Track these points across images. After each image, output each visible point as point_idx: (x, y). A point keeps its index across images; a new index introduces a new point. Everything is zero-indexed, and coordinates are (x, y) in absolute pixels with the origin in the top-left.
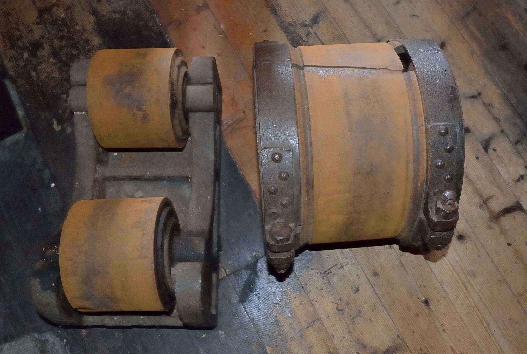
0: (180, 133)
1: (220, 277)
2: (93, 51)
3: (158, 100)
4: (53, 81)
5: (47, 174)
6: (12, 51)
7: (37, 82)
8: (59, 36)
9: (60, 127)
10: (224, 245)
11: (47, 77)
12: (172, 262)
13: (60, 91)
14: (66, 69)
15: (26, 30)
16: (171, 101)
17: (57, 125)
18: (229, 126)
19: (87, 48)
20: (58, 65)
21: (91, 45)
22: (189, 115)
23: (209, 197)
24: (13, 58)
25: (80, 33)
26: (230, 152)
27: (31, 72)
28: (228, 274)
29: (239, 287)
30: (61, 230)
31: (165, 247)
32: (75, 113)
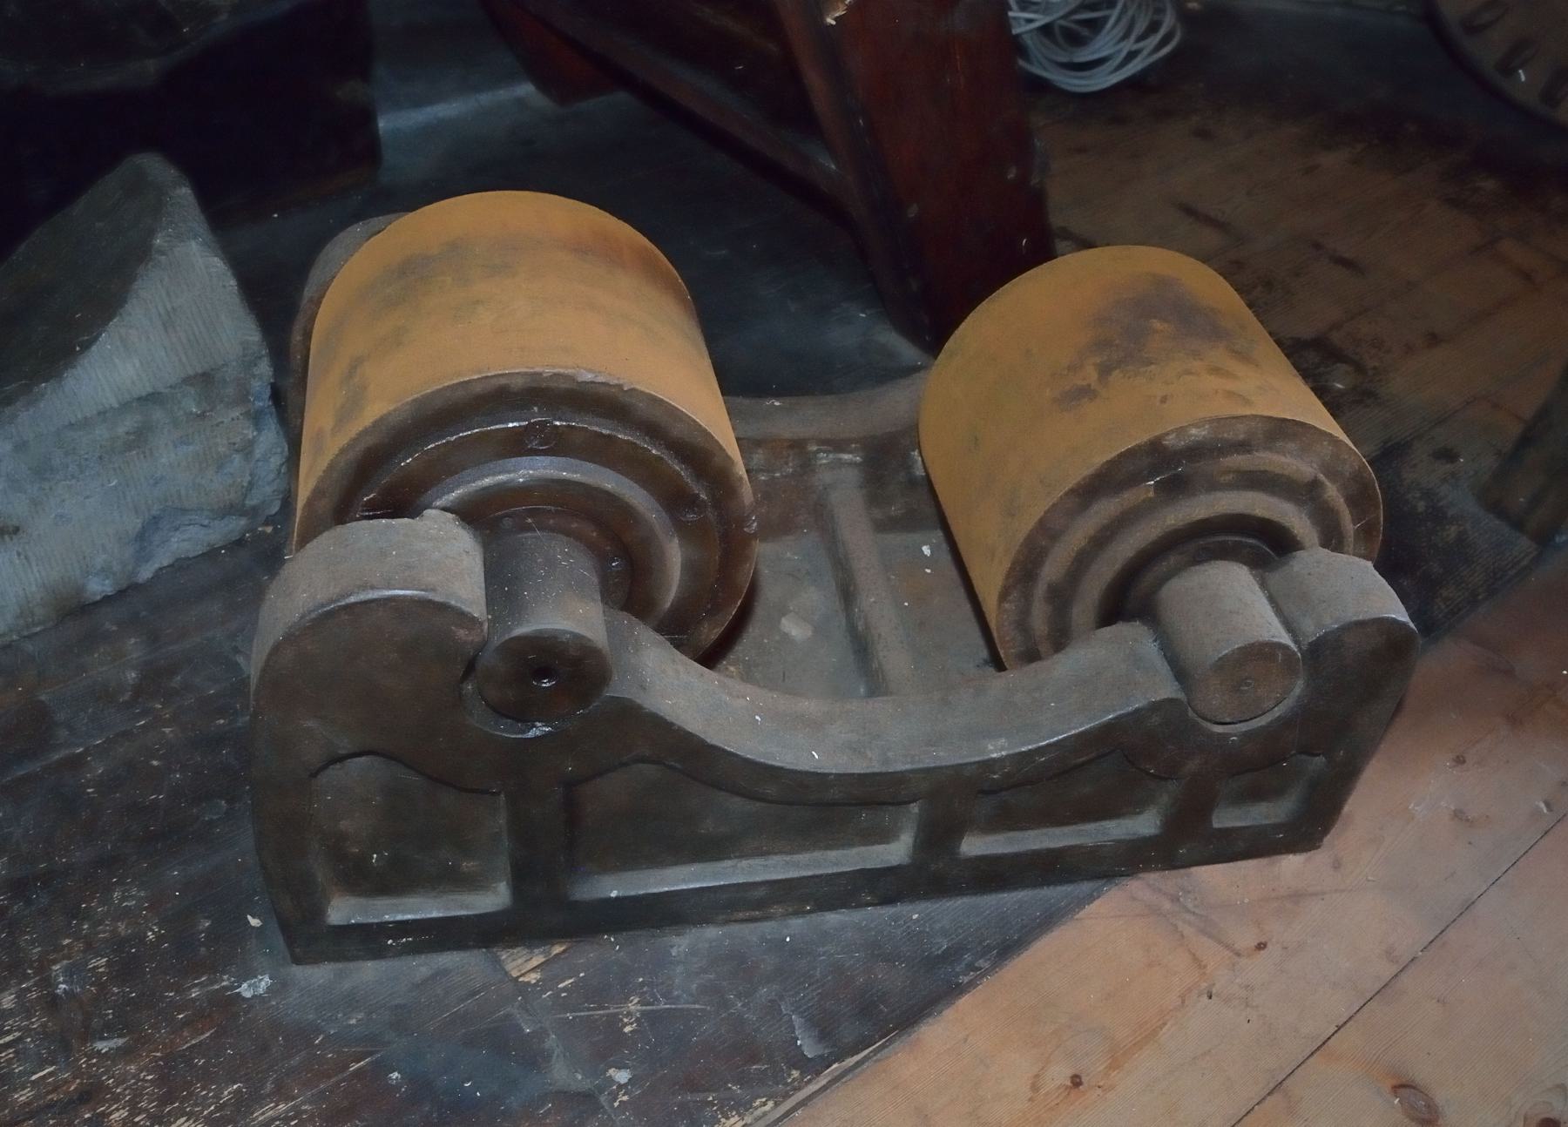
23: (817, 757)
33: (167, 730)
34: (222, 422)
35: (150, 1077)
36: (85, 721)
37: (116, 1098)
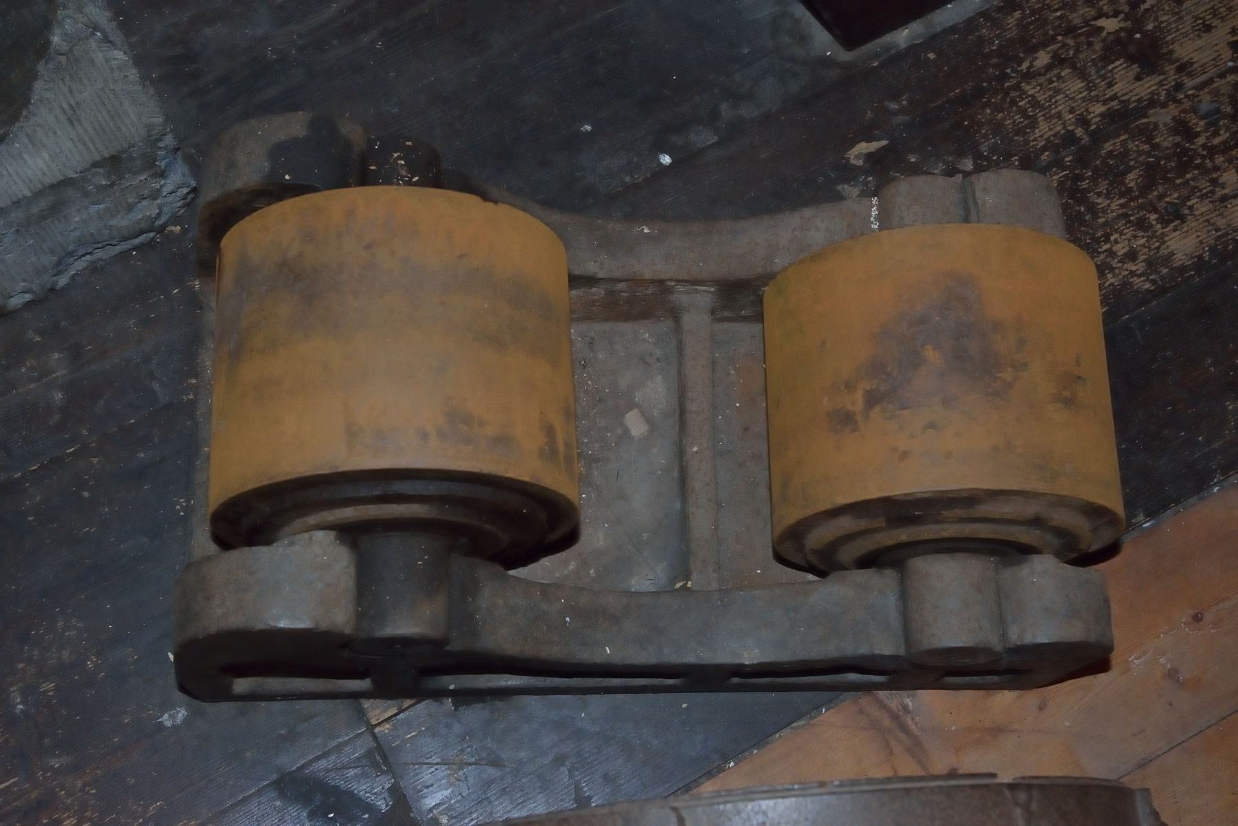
0: (818, 537)
1: (366, 704)
2: (1143, 237)
3: (904, 455)
4: (1021, 122)
5: (703, 137)
7: (1013, 75)
8: (1189, 122)
9: (860, 163)
10: (474, 714)
11: (1035, 103)
12: (350, 533)
13: (984, 149)
14: (1067, 159)
15: (1206, 11)
17: (864, 151)
18: (895, 717)
19: (1153, 217)
20: (1079, 132)
21: (1163, 228)
22: (887, 569)
23: (609, 652)
25: (1209, 189)
26: (801, 723)
27: (1049, 49)
28: (377, 730)
29: (332, 770)
31: (394, 506)
32: (875, 200)
33: (95, 460)
34: (132, 185)
35: (93, 791)
36: (20, 444)
37: (67, 809)
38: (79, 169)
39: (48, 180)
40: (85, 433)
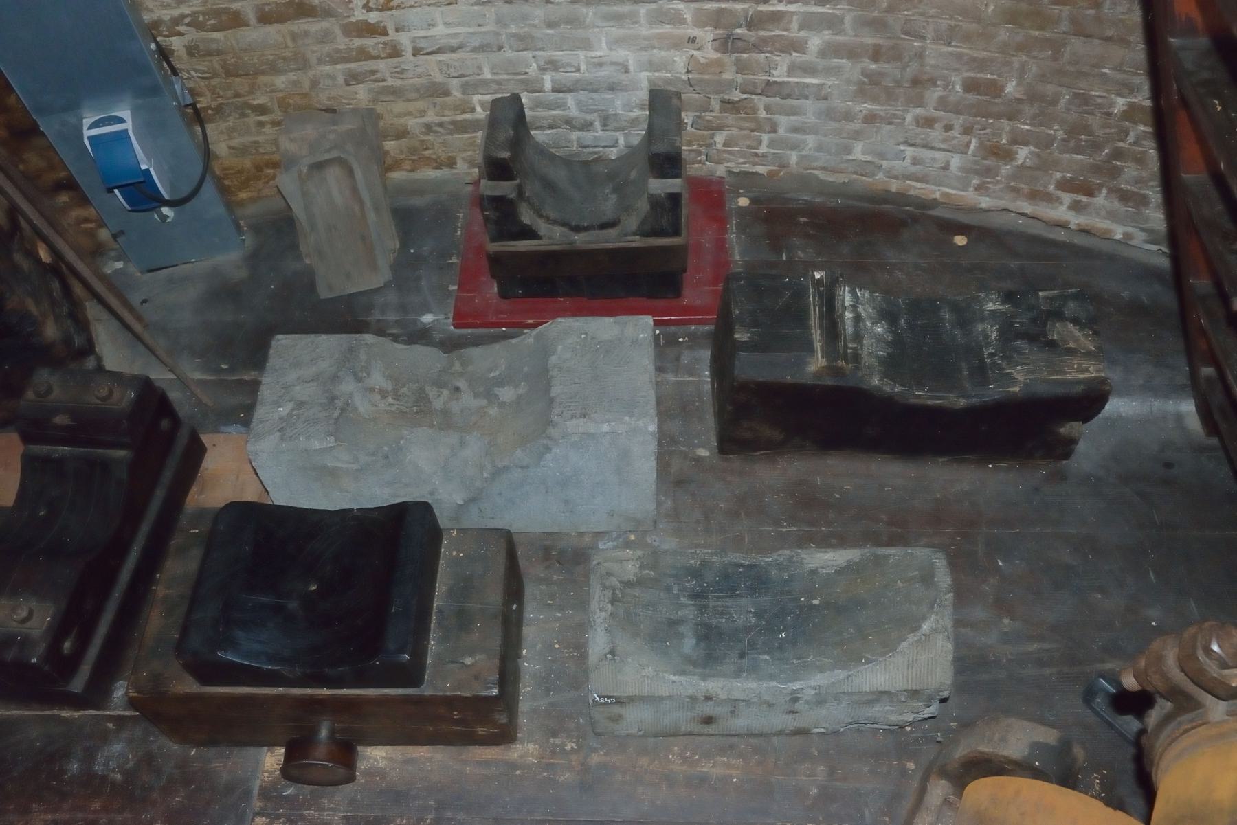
6: (265, 377)
16: (979, 778)
24: (929, 20)
30: (1130, 815)
38: (898, 689)
39: (880, 689)
40: (821, 819)
